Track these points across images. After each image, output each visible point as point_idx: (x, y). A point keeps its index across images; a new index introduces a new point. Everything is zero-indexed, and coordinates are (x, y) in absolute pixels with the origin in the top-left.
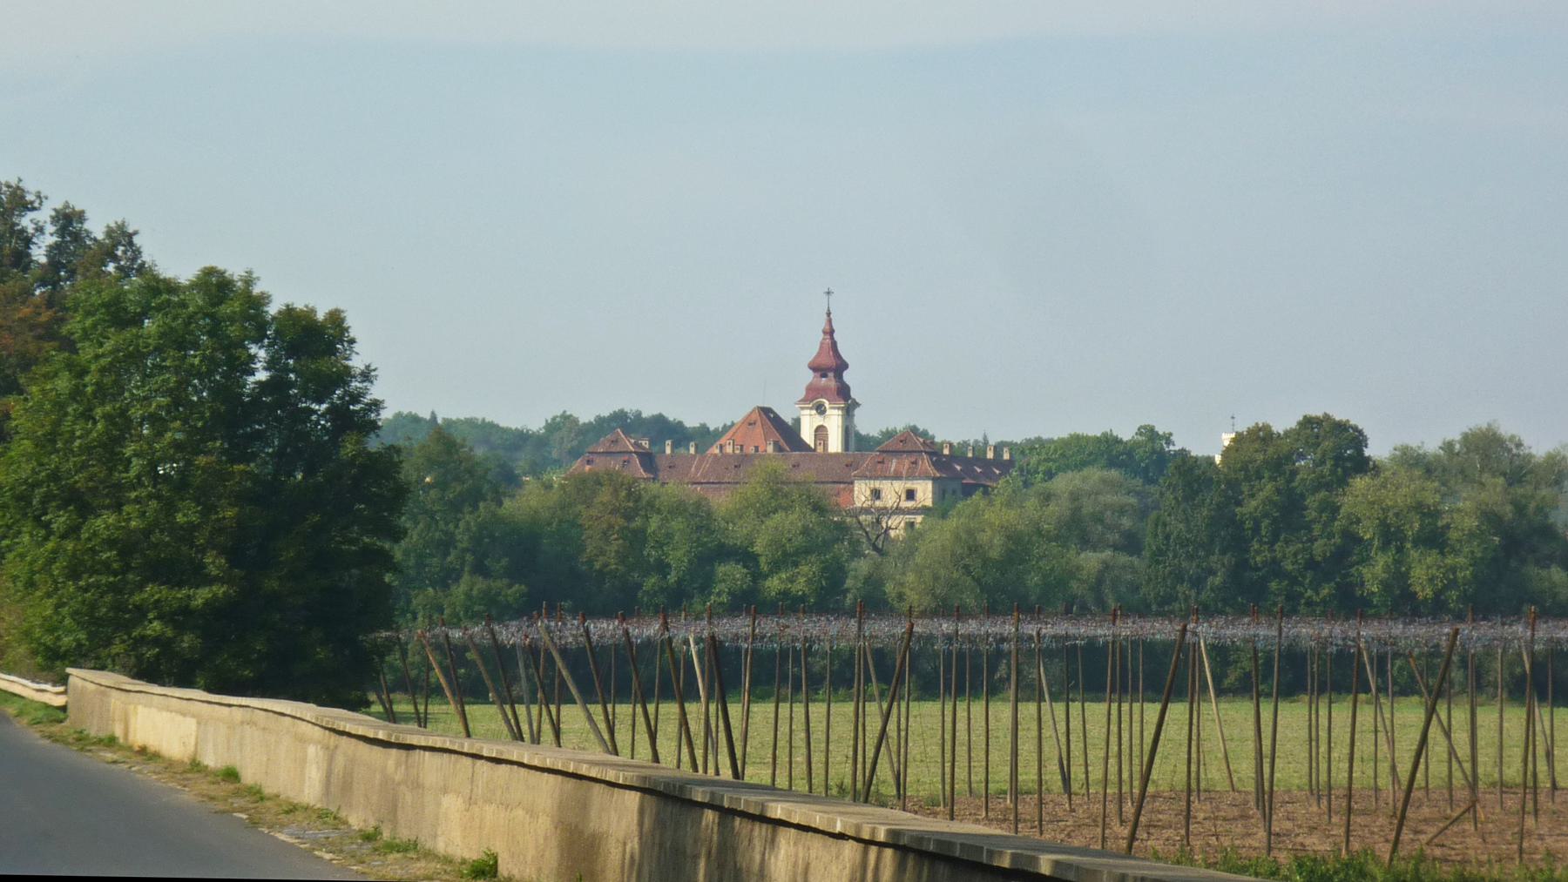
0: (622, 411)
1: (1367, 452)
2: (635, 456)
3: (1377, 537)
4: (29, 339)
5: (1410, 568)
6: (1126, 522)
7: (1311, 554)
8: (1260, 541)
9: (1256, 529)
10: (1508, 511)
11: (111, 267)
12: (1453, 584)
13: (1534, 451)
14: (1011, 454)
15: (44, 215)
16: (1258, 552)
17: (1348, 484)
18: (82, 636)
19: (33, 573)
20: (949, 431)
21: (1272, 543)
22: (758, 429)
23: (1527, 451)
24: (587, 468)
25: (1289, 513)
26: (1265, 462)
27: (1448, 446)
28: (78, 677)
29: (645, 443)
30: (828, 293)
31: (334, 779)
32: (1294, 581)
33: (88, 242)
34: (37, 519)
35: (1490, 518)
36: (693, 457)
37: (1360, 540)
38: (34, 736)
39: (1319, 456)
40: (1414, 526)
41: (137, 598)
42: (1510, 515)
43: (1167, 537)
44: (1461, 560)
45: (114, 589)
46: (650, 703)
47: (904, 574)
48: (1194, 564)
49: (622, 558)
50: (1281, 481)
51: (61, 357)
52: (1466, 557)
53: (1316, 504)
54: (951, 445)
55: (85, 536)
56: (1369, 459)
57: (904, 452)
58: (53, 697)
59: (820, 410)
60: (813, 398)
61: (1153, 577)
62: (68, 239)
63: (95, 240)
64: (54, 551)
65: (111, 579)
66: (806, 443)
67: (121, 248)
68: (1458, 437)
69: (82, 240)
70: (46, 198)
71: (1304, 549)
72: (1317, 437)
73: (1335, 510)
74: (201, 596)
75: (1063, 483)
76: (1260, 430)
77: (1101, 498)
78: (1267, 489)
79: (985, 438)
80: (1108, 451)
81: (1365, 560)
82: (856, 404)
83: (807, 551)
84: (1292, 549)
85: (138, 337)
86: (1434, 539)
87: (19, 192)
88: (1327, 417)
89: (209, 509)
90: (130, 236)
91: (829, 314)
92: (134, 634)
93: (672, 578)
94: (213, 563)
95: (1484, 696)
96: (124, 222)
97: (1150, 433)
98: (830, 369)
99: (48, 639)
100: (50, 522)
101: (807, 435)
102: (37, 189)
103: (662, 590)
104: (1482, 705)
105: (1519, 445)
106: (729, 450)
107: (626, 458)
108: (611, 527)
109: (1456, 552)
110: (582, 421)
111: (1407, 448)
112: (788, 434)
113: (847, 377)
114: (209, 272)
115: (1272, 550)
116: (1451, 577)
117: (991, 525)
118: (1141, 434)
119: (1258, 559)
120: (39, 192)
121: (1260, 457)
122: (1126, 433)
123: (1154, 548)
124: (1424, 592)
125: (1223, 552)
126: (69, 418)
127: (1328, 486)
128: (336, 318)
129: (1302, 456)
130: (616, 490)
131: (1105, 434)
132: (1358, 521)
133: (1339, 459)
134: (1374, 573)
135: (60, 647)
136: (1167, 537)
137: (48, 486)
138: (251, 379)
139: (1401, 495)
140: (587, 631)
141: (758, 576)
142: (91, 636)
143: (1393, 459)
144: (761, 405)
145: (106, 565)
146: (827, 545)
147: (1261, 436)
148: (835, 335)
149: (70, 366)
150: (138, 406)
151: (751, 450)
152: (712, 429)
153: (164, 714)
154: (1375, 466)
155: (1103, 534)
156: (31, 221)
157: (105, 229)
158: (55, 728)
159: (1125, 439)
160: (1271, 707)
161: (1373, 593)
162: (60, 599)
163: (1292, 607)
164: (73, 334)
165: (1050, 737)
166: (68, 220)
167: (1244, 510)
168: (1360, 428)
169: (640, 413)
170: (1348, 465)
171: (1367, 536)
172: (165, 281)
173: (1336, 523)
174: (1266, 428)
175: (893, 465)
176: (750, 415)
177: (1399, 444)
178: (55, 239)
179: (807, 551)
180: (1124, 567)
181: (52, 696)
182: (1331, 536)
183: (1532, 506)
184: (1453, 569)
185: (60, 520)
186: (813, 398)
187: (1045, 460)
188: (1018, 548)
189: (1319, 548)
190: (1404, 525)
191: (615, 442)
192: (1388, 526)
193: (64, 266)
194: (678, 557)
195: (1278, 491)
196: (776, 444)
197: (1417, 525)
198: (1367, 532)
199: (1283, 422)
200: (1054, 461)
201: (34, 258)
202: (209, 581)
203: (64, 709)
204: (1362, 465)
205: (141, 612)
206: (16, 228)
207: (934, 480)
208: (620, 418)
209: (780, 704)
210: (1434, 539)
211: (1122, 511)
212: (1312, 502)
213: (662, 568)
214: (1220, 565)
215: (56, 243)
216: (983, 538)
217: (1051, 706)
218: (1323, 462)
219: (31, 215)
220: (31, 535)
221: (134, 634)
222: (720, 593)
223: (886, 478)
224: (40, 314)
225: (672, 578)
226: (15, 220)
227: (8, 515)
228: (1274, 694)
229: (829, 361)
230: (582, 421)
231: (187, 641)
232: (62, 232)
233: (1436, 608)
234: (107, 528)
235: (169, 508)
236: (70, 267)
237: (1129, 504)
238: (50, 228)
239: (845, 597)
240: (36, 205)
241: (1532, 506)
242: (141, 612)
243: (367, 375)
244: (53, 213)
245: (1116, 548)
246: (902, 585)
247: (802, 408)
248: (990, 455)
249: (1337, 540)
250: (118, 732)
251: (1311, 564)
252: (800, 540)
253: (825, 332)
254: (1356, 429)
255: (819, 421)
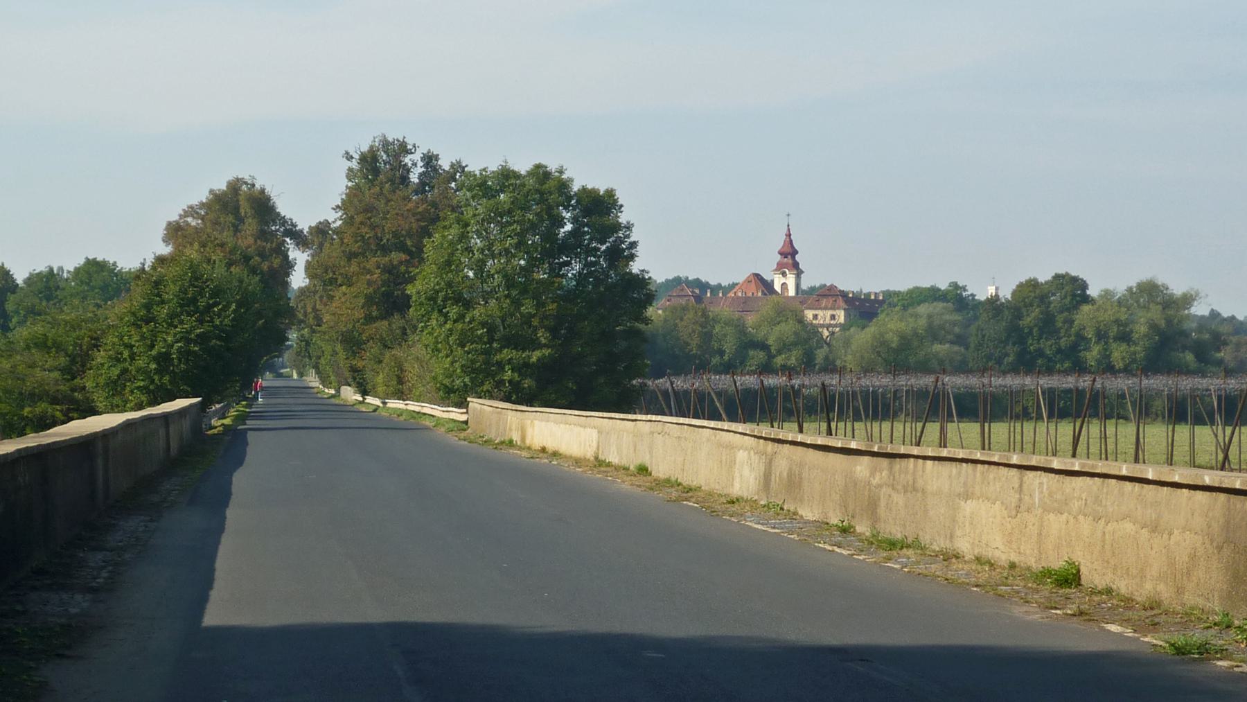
0: (678, 276)
1: (1088, 292)
2: (692, 298)
3: (1094, 336)
4: (413, 221)
5: (1111, 352)
6: (957, 330)
7: (1059, 345)
8: (1033, 340)
9: (1030, 333)
10: (1163, 324)
11: (453, 185)
12: (1134, 361)
13: (1175, 292)
14: (883, 297)
15: (417, 157)
16: (1032, 345)
17: (1079, 309)
18: (467, 380)
19: (437, 343)
20: (849, 285)
21: (1039, 340)
22: (753, 285)
23: (1171, 292)
24: (668, 303)
25: (1047, 325)
26: (1035, 297)
27: (1130, 289)
28: (474, 403)
29: (697, 291)
30: (788, 215)
31: (775, 478)
32: (1050, 360)
33: (440, 171)
34: (440, 311)
35: (1153, 326)
36: (722, 298)
37: (1086, 338)
38: (452, 438)
39: (1063, 294)
40: (1114, 331)
41: (498, 357)
42: (1164, 325)
43: (984, 336)
44: (1138, 348)
45: (487, 353)
46: (776, 422)
47: (845, 356)
48: (998, 351)
49: (699, 346)
50: (1043, 308)
51: (453, 216)
52: (1141, 347)
53: (1062, 319)
54: (853, 292)
55: (467, 320)
56: (1089, 296)
57: (830, 295)
58: (459, 415)
59: (784, 274)
60: (780, 269)
61: (976, 357)
62: (430, 169)
63: (444, 170)
64: (450, 330)
65: (484, 346)
66: (775, 290)
67: (458, 174)
68: (1135, 285)
69: (437, 170)
70: (418, 147)
71: (1056, 343)
72: (1062, 284)
73: (1071, 322)
74: (535, 356)
75: (923, 309)
76: (1032, 281)
77: (944, 317)
78: (1036, 312)
79: (861, 290)
80: (933, 294)
81: (1088, 349)
82: (802, 272)
83: (795, 344)
84: (1049, 343)
85: (498, 204)
86: (1125, 337)
87: (404, 144)
88: (1067, 274)
89: (541, 305)
90: (464, 168)
91: (788, 226)
92: (496, 379)
93: (726, 358)
94: (543, 336)
95: (1150, 420)
96: (460, 160)
97: (955, 286)
98: (789, 254)
99: (447, 382)
100: (448, 312)
101: (777, 287)
102: (413, 142)
103: (721, 364)
104: (1148, 424)
105: (1167, 289)
106: (740, 294)
107: (687, 298)
108: (694, 331)
109: (1136, 344)
110: (658, 282)
111: (1108, 290)
112: (768, 286)
113: (798, 258)
114: (538, 166)
115: (1038, 343)
116: (1134, 357)
117: (891, 330)
118: (950, 286)
119: (1031, 348)
120: (415, 144)
121: (1033, 295)
122: (943, 286)
123: (976, 342)
124: (1119, 365)
125: (1014, 344)
126: (458, 252)
127: (1068, 310)
128: (610, 193)
129: (1054, 294)
130: (696, 312)
131: (932, 286)
132: (1084, 329)
133: (1074, 296)
134: (1092, 355)
135: (454, 386)
136: (984, 336)
137: (447, 291)
138: (562, 230)
139: (1107, 316)
140: (762, 381)
141: (771, 357)
142: (472, 380)
143: (1100, 296)
144: (754, 272)
145: (480, 337)
146: (806, 341)
147: (1032, 284)
148: (792, 237)
149: (458, 221)
150: (499, 245)
151: (750, 295)
152: (723, 285)
153: (562, 426)
154: (1092, 300)
155: (945, 336)
156: (410, 160)
157: (450, 164)
158: (462, 435)
159: (943, 289)
160: (1020, 424)
161: (1092, 366)
162: (454, 358)
163: (1050, 371)
164: (461, 202)
165: (1027, 443)
166: (430, 159)
167: (1024, 323)
168: (1085, 279)
169: (688, 278)
170: (1078, 299)
171: (1090, 336)
172: (513, 172)
173: (1073, 329)
174: (1035, 280)
175: (824, 302)
176: (749, 277)
177: (1103, 288)
178: (423, 169)
179: (795, 344)
180: (956, 353)
181: (457, 414)
182: (1070, 336)
183: (1176, 321)
184: (1135, 353)
185: (453, 311)
186: (780, 269)
187: (902, 300)
188: (907, 342)
189: (1063, 342)
190: (1109, 330)
191: (682, 290)
192: (1101, 330)
193: (428, 184)
194: (729, 347)
195: (1042, 313)
196: (763, 291)
197: (1115, 330)
198: (1089, 334)
199: (1044, 276)
200: (907, 300)
201: (412, 180)
202: (541, 346)
203: (466, 422)
204: (1086, 299)
205: (501, 365)
206: (403, 163)
207: (845, 309)
208: (677, 281)
209: (1146, 426)
210: (1125, 337)
211: (954, 324)
212: (1060, 318)
213: (721, 353)
214: (1012, 351)
215: (423, 172)
216: (889, 336)
217: (958, 425)
218: (1065, 297)
219: (410, 156)
220: (437, 320)
221: (496, 379)
222: (752, 364)
223: (820, 309)
224: (418, 207)
225: (726, 358)
226: (402, 159)
227: (423, 309)
228: (835, 420)
229: (789, 250)
230: (658, 282)
231: (527, 383)
232: (426, 165)
233: (1127, 371)
234: (480, 315)
235: (517, 303)
236: (432, 184)
237: (959, 320)
238: (420, 164)
239: (815, 367)
240: (413, 151)
241: (1176, 321)
242: (501, 365)
243: (629, 227)
244: (422, 155)
245: (952, 342)
246: (845, 361)
247: (775, 274)
248: (873, 297)
249: (1073, 338)
250: (516, 437)
251: (1059, 351)
252: (792, 338)
253: (786, 235)
254: (1082, 280)
255: (783, 280)
